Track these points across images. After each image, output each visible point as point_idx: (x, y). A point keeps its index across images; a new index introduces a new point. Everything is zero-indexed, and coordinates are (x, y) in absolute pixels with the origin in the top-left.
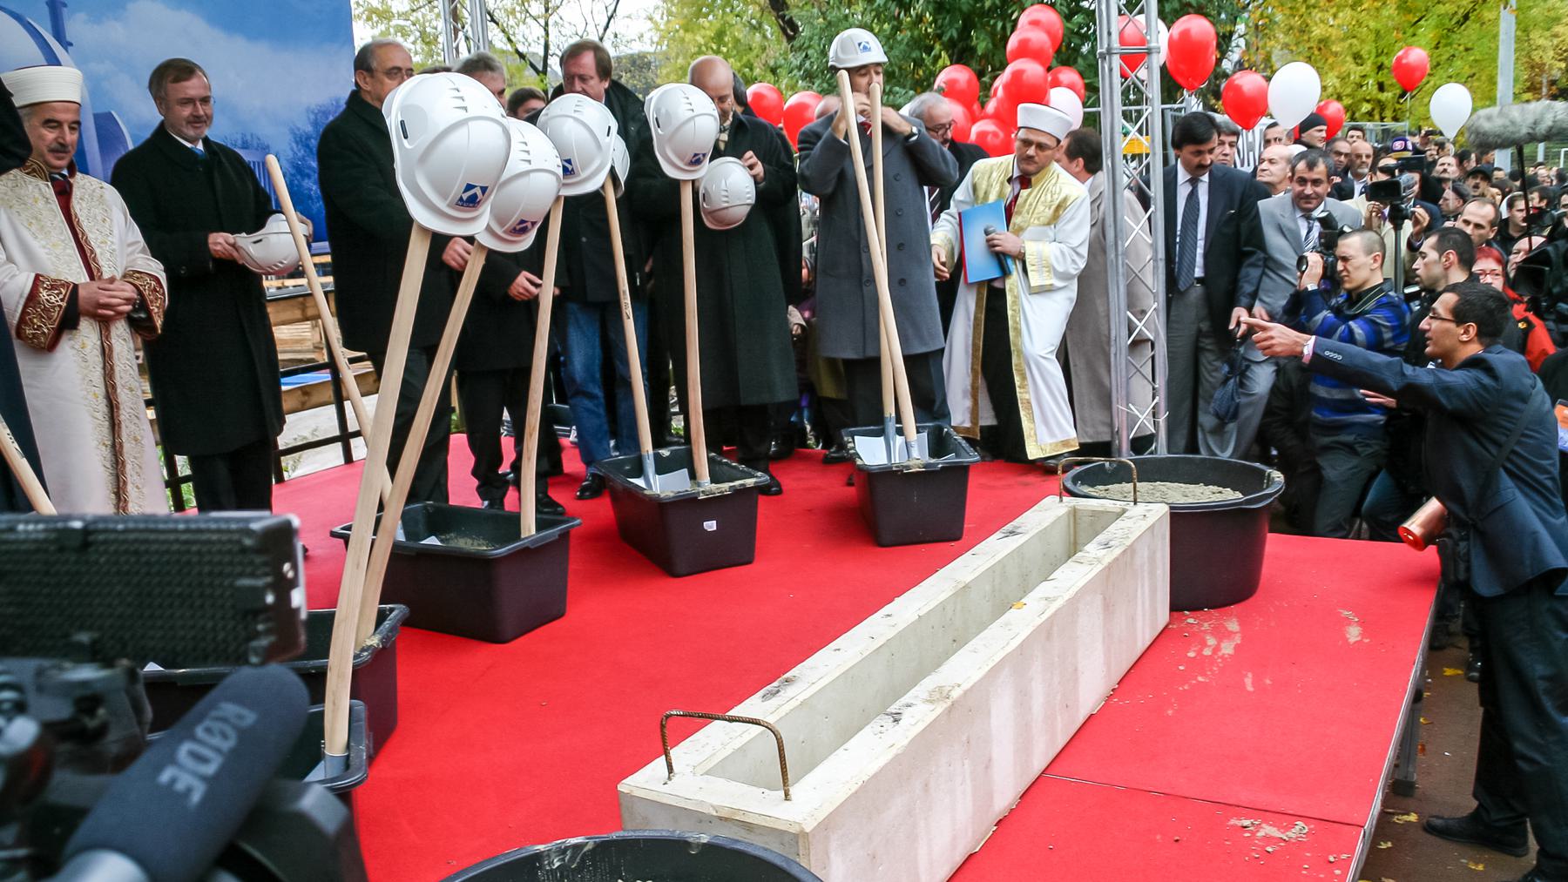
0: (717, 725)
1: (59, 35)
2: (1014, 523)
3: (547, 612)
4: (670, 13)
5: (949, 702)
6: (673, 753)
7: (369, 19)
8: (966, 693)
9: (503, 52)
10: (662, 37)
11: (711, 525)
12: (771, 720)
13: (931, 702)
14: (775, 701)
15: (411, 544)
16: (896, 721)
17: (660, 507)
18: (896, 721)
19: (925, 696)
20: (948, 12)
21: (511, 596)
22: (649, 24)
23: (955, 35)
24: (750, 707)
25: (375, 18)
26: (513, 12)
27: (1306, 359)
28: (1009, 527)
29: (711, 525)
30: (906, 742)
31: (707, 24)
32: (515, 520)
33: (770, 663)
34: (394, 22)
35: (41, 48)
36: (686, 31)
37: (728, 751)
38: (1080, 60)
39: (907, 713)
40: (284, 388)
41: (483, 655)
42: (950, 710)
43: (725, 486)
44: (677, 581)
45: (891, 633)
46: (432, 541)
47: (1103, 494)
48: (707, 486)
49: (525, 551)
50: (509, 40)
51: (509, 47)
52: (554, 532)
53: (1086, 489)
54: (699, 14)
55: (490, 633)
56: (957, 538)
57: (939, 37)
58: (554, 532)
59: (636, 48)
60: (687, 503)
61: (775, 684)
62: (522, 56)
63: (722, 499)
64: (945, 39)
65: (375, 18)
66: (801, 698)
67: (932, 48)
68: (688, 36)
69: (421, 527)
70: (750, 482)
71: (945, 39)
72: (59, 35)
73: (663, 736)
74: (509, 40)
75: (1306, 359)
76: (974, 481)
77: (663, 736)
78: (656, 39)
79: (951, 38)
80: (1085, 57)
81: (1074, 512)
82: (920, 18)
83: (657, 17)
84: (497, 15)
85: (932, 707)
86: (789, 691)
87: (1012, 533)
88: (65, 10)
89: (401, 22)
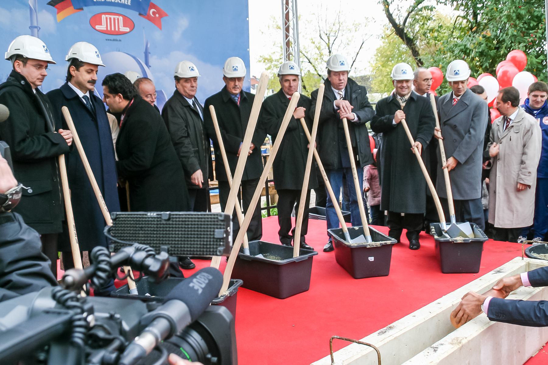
0: (354, 345)
1: (147, 63)
2: (500, 267)
3: (302, 288)
4: (377, 60)
5: (461, 345)
6: (335, 354)
7: (264, 62)
8: (469, 341)
9: (313, 74)
10: (374, 69)
11: (371, 259)
12: (377, 346)
13: (452, 344)
14: (383, 336)
15: (252, 256)
16: (435, 351)
17: (351, 250)
18: (435, 351)
19: (450, 341)
20: (485, 56)
21: (287, 280)
22: (369, 64)
23: (488, 65)
24: (371, 338)
25: (266, 61)
26: (317, 59)
27: (381, 134)
28: (498, 269)
29: (371, 259)
30: (438, 361)
31: (391, 64)
32: (292, 250)
33: (383, 318)
34: (274, 63)
35: (141, 68)
36: (383, 67)
37: (360, 356)
38: (541, 75)
39: (440, 348)
40: (211, 194)
41: (273, 303)
42: (460, 349)
43: (378, 244)
44: (356, 280)
45: (439, 311)
46: (260, 256)
47: (543, 258)
48: (370, 242)
49: (294, 263)
50: (315, 70)
51: (315, 73)
52: (306, 256)
53: (535, 255)
54: (388, 60)
55: (276, 294)
56: (477, 272)
57: (481, 66)
58: (306, 256)
59: (363, 74)
60: (363, 249)
61: (385, 328)
62: (320, 76)
63: (377, 248)
64: (484, 67)
65: (266, 61)
66: (395, 336)
67: (478, 71)
68: (384, 69)
69: (257, 250)
70: (389, 242)
71: (484, 67)
72: (147, 63)
73: (330, 346)
74: (315, 70)
75: (381, 134)
76: (485, 246)
77: (330, 346)
78: (371, 70)
79: (486, 67)
80: (544, 74)
81: (529, 264)
82: (473, 59)
83: (372, 62)
84: (311, 60)
85: (452, 346)
86: (390, 332)
87: (499, 272)
88: (149, 55)
89: (276, 63)
